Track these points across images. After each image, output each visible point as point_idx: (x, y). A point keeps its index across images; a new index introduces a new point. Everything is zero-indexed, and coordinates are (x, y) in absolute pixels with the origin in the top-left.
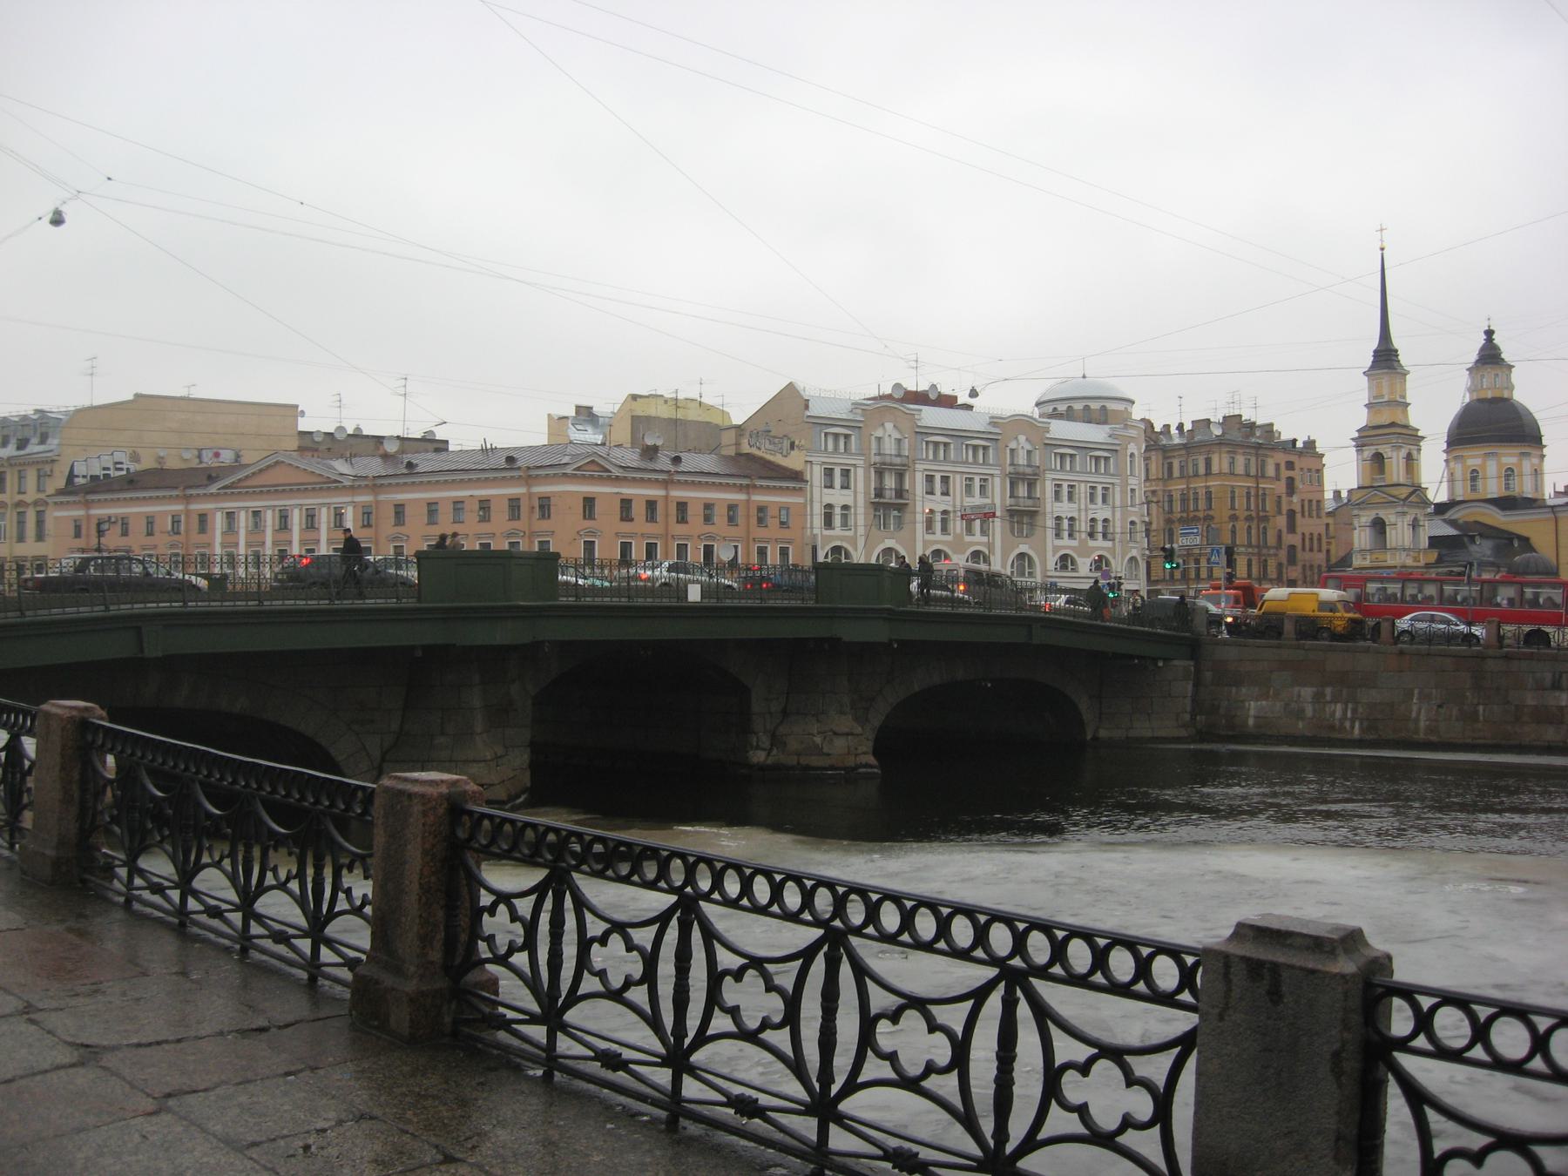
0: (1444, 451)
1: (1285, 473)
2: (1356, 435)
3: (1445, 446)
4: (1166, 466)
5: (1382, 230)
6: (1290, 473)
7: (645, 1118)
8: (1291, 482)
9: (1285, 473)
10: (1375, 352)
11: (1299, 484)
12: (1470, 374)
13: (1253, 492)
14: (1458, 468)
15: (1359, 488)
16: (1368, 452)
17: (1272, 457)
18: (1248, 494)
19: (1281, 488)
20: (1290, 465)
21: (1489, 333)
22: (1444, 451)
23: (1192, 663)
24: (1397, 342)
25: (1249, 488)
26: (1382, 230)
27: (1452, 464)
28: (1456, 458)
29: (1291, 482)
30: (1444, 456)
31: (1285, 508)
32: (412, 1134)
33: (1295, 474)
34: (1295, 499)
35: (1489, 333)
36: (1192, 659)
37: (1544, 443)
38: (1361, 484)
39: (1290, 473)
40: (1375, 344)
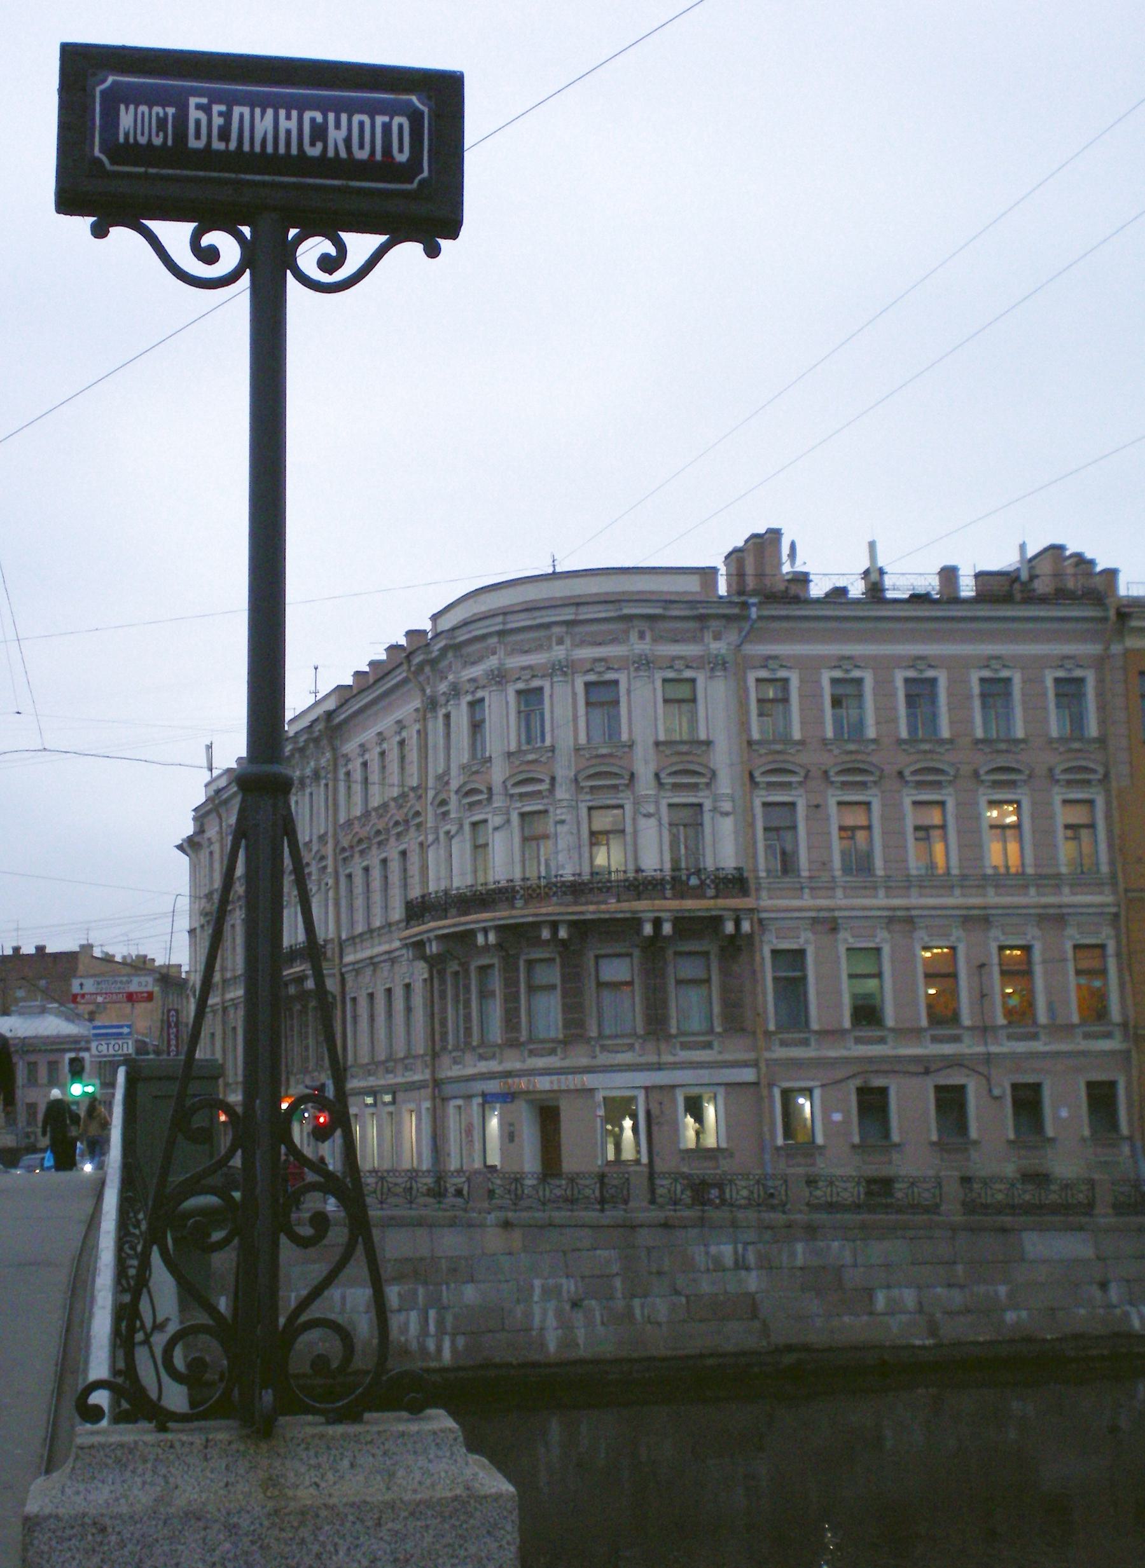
21: (872, 546)
35: (872, 546)
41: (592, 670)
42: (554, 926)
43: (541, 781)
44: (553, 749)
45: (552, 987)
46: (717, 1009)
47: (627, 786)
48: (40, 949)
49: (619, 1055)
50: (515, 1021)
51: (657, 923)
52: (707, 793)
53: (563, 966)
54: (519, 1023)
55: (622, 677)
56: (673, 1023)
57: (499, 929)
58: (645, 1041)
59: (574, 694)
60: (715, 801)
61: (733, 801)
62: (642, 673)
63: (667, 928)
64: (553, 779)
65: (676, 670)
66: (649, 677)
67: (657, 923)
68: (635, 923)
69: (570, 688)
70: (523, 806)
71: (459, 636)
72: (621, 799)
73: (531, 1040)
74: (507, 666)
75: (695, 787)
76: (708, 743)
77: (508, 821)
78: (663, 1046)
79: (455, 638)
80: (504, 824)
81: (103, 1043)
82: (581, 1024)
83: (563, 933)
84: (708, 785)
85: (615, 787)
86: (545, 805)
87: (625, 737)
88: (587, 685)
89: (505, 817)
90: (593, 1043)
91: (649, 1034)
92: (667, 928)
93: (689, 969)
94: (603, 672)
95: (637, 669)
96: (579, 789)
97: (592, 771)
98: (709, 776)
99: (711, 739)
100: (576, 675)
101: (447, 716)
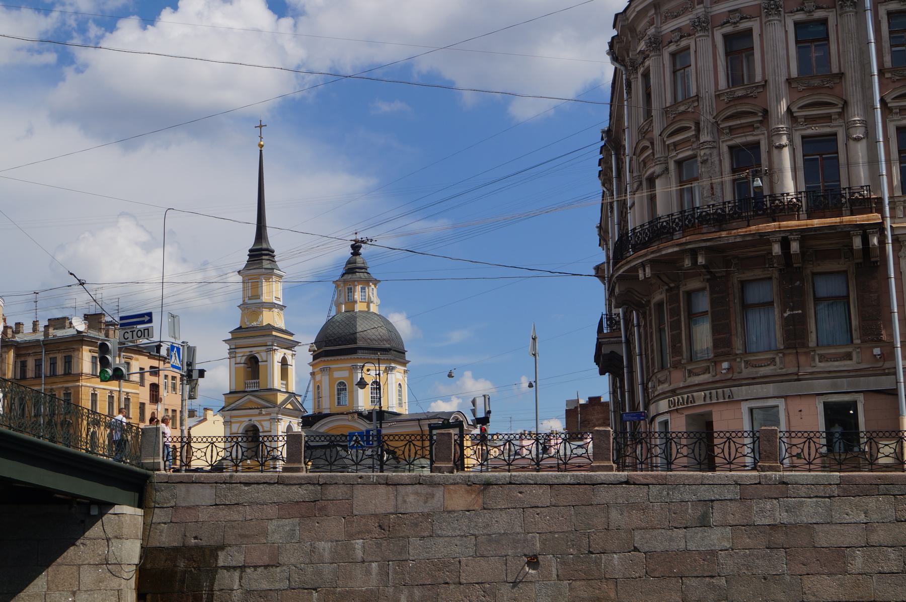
0: (310, 364)
1: (150, 379)
2: (230, 336)
3: (310, 358)
4: (19, 365)
5: (261, 126)
6: (154, 380)
7: (385, 107)
8: (154, 388)
9: (150, 379)
10: (251, 251)
11: (163, 392)
12: (337, 287)
13: (115, 395)
14: (325, 380)
15: (231, 393)
16: (241, 358)
17: (137, 360)
18: (111, 397)
19: (144, 394)
20: (155, 371)
22: (310, 364)
23: (140, 512)
24: (274, 240)
25: (111, 392)
26: (261, 126)
27: (318, 377)
28: (322, 370)
29: (154, 388)
30: (310, 369)
31: (148, 416)
32: (874, 560)
33: (161, 381)
34: (160, 407)
36: (139, 506)
37: (408, 356)
38: (234, 388)
39: (154, 380)
40: (250, 241)
41: (728, 22)
42: (694, 253)
43: (689, 128)
44: (697, 97)
45: (706, 313)
46: (855, 323)
47: (761, 122)
48: (602, 373)
49: (762, 369)
50: (678, 345)
51: (785, 244)
52: (839, 122)
53: (712, 293)
54: (681, 347)
55: (755, 25)
56: (813, 338)
57: (653, 262)
58: (784, 355)
59: (714, 46)
60: (847, 129)
61: (866, 127)
62: (771, 18)
63: (795, 247)
64: (697, 124)
65: (806, 12)
66: (780, 21)
67: (785, 244)
68: (763, 239)
69: (710, 39)
70: (677, 154)
71: (630, 16)
72: (757, 135)
73: (691, 360)
74: (663, 33)
75: (828, 118)
76: (841, 75)
77: (667, 169)
78: (802, 359)
79: (628, 19)
80: (664, 171)
81: (129, 331)
82: (728, 343)
83: (701, 260)
84: (841, 114)
85: (751, 126)
86: (693, 150)
87: (758, 78)
88: (726, 37)
89: (664, 166)
90: (738, 360)
91: (786, 348)
92: (795, 247)
93: (827, 287)
94: (738, 22)
95: (768, 15)
96: (720, 131)
97: (729, 112)
98: (841, 106)
99: (842, 71)
100: (715, 29)
101: (646, 76)
